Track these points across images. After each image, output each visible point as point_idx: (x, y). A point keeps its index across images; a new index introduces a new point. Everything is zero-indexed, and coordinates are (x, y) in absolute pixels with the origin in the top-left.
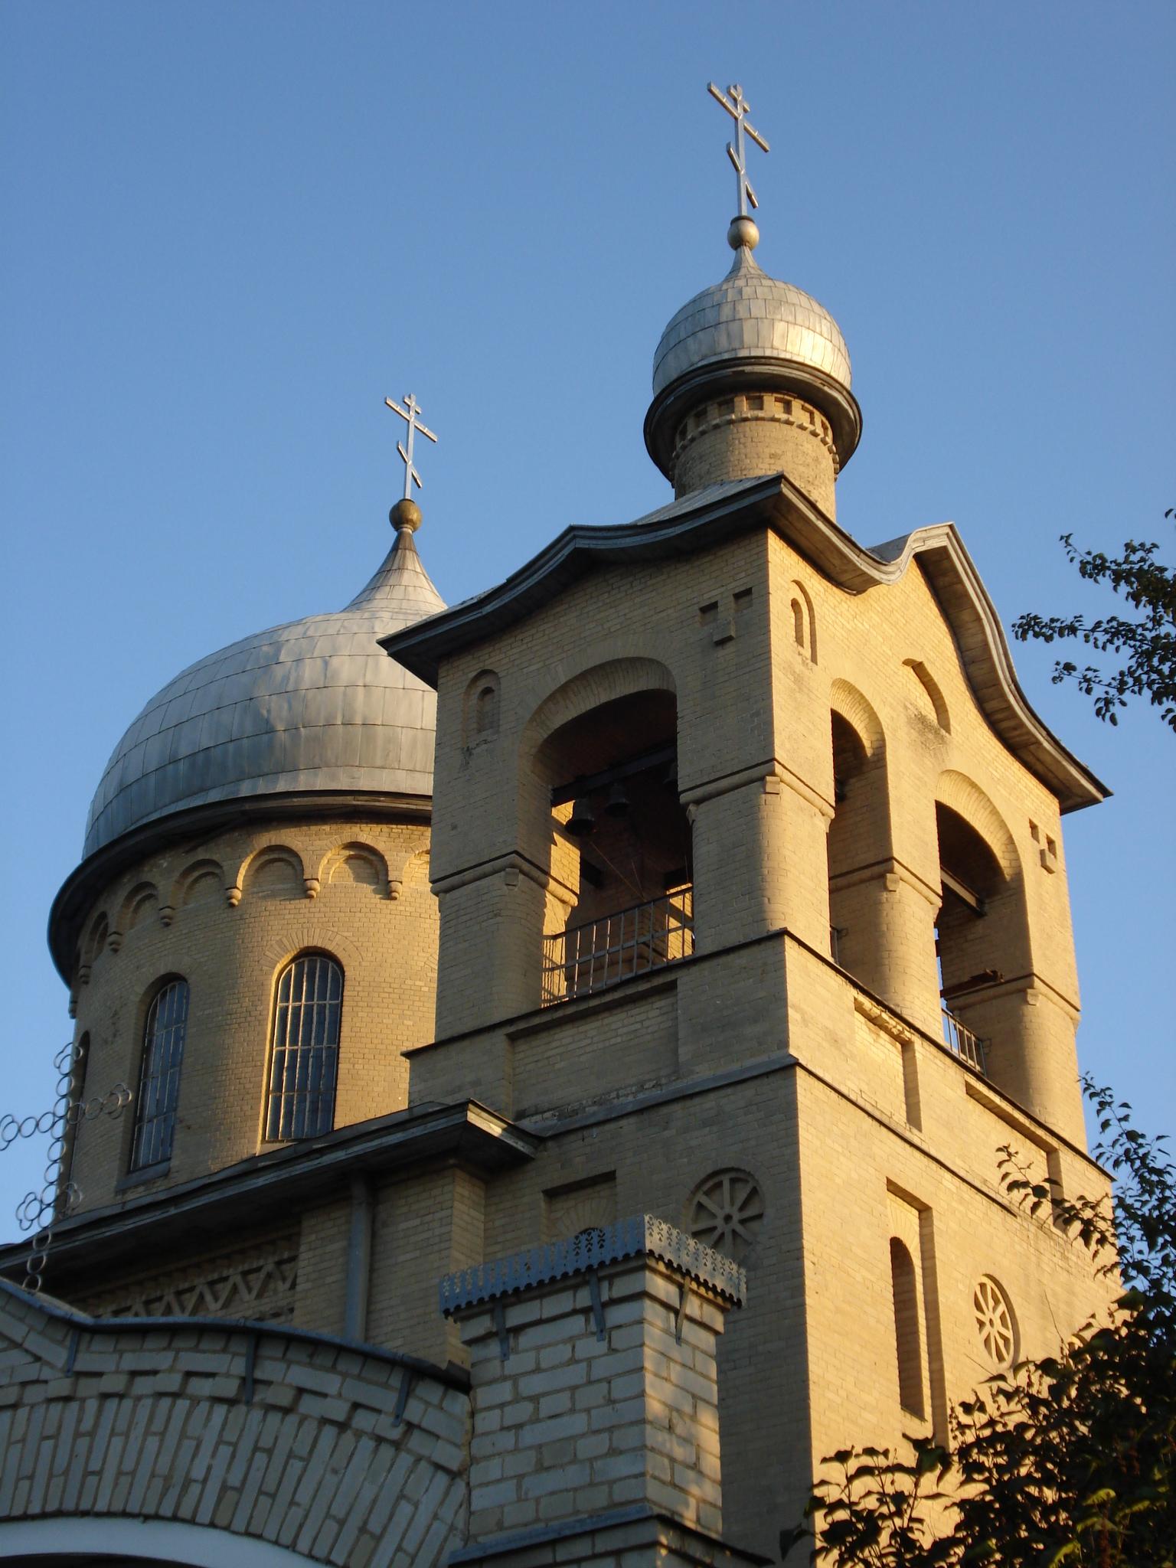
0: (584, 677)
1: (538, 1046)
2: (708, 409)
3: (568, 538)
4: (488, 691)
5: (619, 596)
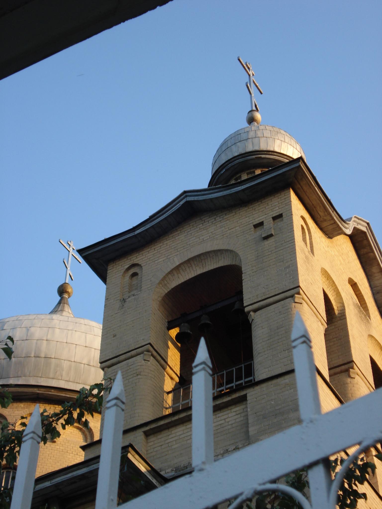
0: (189, 262)
1: (161, 438)
2: (242, 176)
3: (182, 197)
4: (135, 275)
5: (208, 225)
